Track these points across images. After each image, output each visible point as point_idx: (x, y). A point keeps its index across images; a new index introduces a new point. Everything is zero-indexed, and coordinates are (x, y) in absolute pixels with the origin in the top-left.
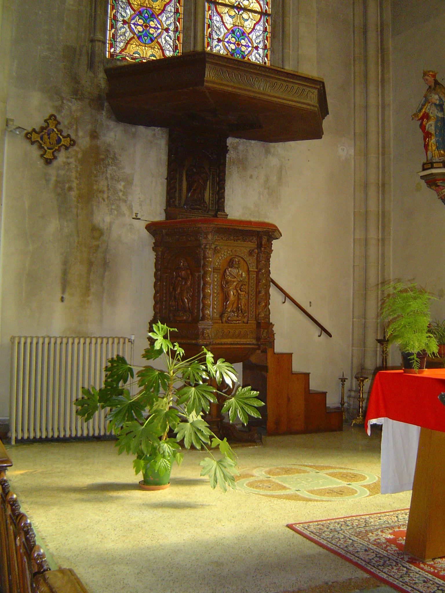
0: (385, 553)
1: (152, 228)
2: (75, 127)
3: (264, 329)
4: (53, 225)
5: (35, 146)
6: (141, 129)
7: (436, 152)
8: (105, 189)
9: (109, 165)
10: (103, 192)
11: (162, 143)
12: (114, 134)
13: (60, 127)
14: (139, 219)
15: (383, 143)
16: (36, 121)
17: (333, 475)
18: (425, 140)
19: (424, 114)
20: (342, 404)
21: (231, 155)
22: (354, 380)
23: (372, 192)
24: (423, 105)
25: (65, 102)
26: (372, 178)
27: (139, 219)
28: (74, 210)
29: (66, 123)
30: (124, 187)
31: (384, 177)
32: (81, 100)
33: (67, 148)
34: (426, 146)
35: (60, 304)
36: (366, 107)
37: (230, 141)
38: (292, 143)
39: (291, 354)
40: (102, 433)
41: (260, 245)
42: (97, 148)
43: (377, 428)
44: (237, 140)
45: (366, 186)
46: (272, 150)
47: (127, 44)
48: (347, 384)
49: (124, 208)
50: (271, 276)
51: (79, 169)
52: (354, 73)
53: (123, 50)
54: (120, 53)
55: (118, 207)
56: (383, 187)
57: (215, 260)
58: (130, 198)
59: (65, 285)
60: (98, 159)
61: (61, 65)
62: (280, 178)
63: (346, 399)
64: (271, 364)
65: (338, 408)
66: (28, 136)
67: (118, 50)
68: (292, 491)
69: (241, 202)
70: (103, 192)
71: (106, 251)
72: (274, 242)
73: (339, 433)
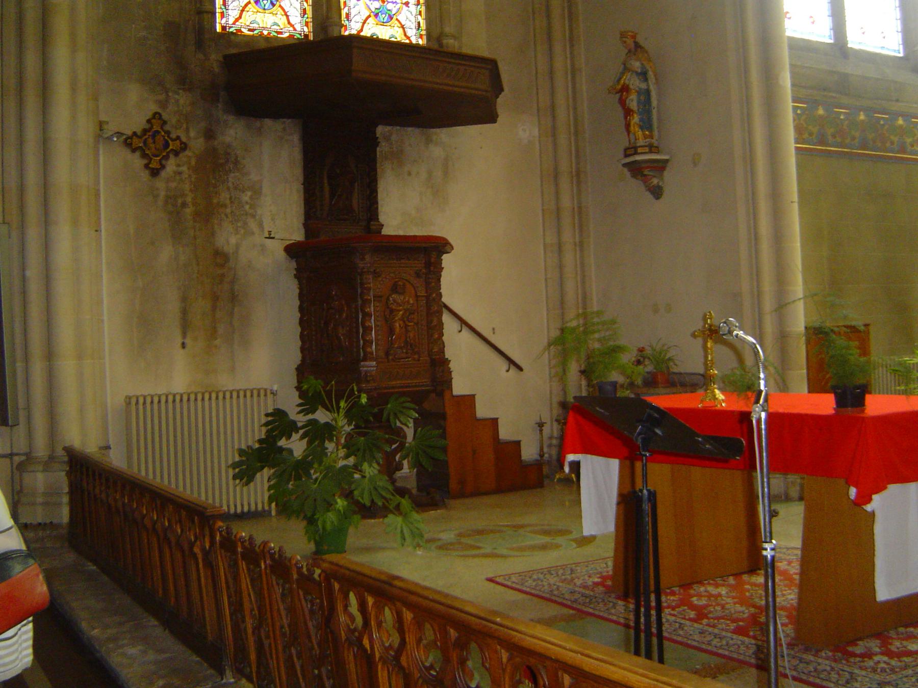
0: (592, 593)
1: (292, 250)
2: (185, 126)
3: (439, 368)
4: (166, 253)
5: (138, 154)
6: (268, 122)
7: (640, 133)
8: (228, 202)
9: (230, 171)
10: (225, 206)
11: (296, 138)
12: (234, 132)
13: (167, 128)
14: (273, 238)
15: (576, 119)
16: (136, 122)
17: (535, 532)
18: (626, 118)
19: (623, 86)
20: (542, 456)
21: (383, 149)
22: (555, 424)
23: (565, 184)
24: (623, 73)
25: (170, 94)
26: (564, 166)
27: (273, 238)
28: (192, 233)
29: (174, 121)
30: (251, 197)
31: (578, 163)
32: (190, 90)
33: (177, 154)
34: (628, 126)
35: (182, 351)
36: (551, 72)
37: (381, 130)
38: (459, 129)
39: (474, 396)
40: (246, 509)
41: (428, 264)
42: (214, 150)
43: (576, 466)
44: (388, 128)
45: (556, 176)
46: (434, 137)
47: (242, 11)
48: (546, 430)
49: (253, 225)
50: (444, 299)
51: (193, 179)
52: (534, 30)
53: (237, 20)
54: (234, 24)
55: (245, 223)
56: (578, 176)
57: (375, 286)
58: (259, 212)
59: (185, 326)
60: (217, 165)
61: (163, 48)
62: (446, 173)
63: (545, 450)
64: (449, 410)
65: (537, 460)
66: (128, 142)
67: (231, 21)
68: (488, 550)
69: (401, 209)
70: (225, 206)
71: (233, 282)
72: (445, 257)
73: (538, 490)
